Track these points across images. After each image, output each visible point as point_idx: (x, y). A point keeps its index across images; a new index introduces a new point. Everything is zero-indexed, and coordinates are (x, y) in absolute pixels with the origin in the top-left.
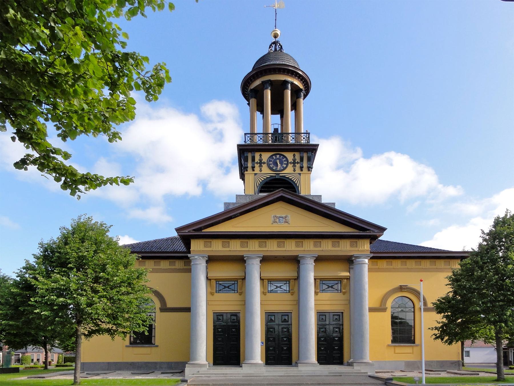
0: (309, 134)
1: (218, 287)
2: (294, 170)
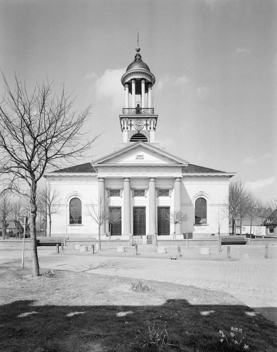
0: (153, 108)
1: (111, 193)
2: (147, 129)
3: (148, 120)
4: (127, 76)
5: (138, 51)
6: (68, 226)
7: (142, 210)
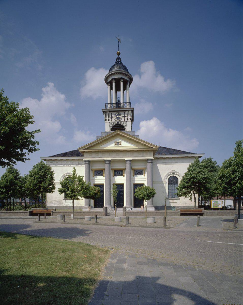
0: (130, 103)
2: (125, 120)
3: (125, 112)
4: (108, 78)
5: (119, 54)
6: (63, 200)
7: (121, 186)
